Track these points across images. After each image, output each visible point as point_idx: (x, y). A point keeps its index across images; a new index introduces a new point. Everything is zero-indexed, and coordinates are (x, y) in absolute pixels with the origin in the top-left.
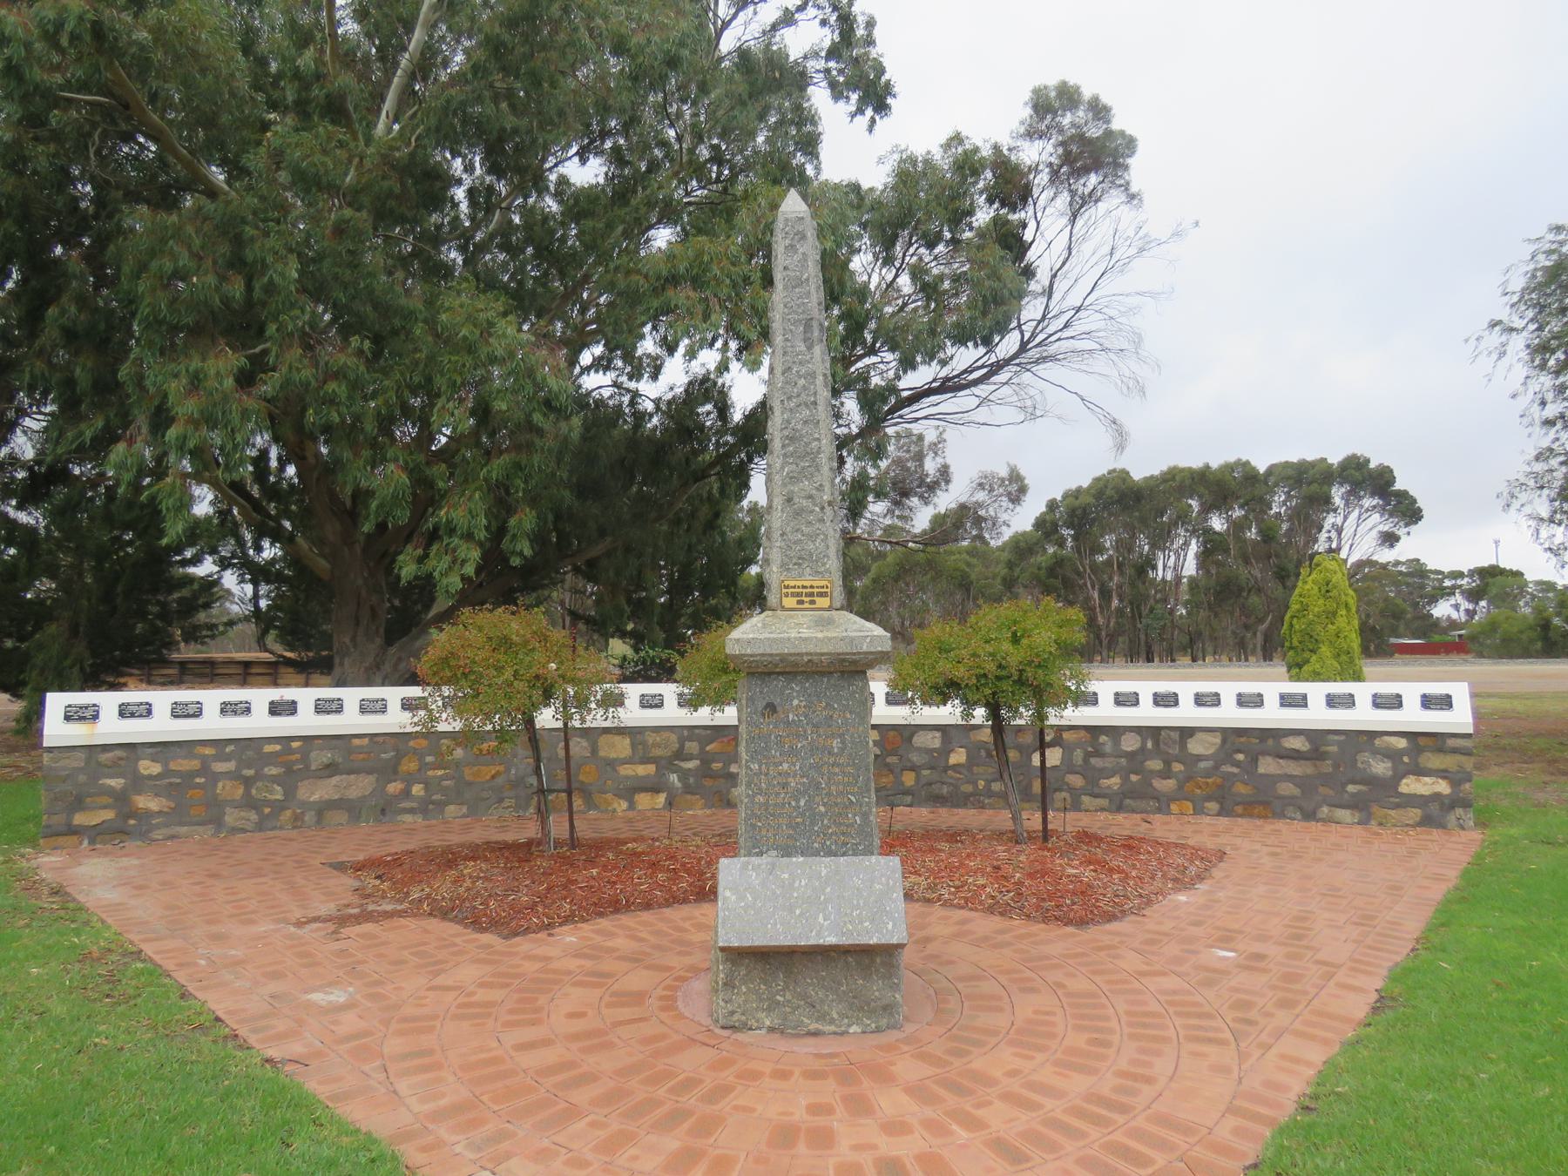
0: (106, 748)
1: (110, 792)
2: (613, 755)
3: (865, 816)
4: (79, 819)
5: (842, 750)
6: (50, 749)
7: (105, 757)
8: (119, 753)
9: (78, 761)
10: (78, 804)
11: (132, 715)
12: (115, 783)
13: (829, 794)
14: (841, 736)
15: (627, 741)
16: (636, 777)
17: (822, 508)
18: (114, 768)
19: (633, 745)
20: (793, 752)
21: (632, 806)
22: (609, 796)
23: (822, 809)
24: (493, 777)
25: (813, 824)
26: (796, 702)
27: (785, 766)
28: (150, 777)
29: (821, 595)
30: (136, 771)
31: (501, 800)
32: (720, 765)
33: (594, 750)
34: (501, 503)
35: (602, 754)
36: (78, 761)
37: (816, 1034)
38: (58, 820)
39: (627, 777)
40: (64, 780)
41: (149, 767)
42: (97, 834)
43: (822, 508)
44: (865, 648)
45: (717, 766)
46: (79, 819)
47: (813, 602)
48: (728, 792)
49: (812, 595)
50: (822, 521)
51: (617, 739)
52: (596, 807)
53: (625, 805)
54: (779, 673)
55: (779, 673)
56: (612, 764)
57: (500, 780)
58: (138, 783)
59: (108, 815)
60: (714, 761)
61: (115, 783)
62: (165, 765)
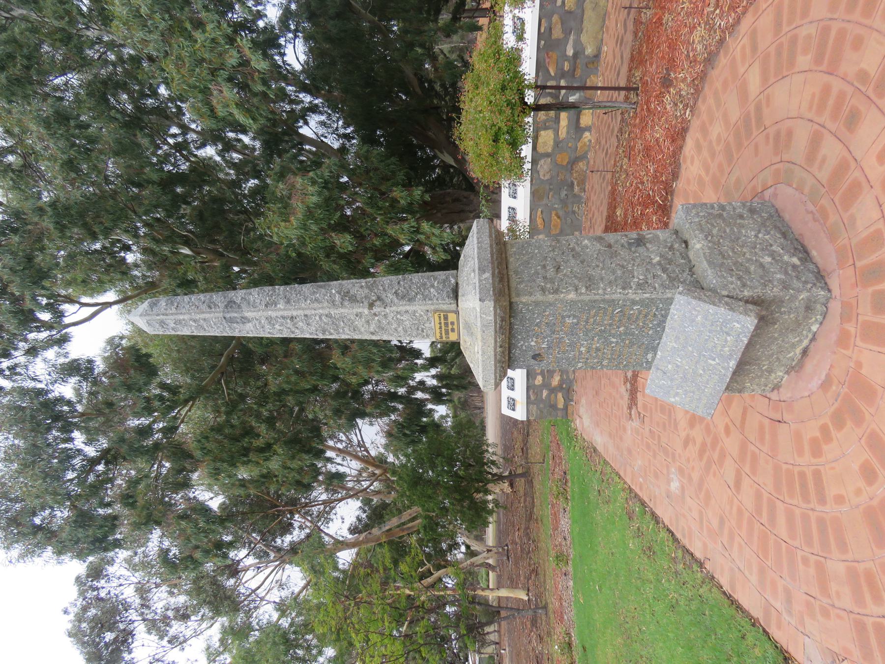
0: (528, 397)
1: (549, 396)
2: (552, 143)
3: (634, 303)
4: (561, 405)
5: (575, 317)
6: (527, 417)
7: (532, 398)
8: (531, 393)
9: (534, 408)
10: (554, 407)
11: (513, 386)
12: (545, 393)
13: (610, 325)
14: (563, 317)
15: (542, 133)
16: (568, 126)
17: (375, 315)
18: (538, 393)
19: (546, 128)
20: (572, 345)
21: (588, 129)
22: (579, 145)
23: (622, 329)
24: (559, 217)
25: (633, 334)
26: (533, 343)
27: (583, 349)
28: (543, 380)
29: (446, 318)
30: (539, 386)
31: (574, 212)
32: (566, 64)
33: (547, 155)
34: (394, 212)
35: (550, 150)
36: (534, 408)
37: (805, 352)
38: (560, 413)
39: (568, 133)
40: (542, 412)
41: (539, 380)
42: (568, 399)
43: (375, 315)
44: (492, 318)
45: (567, 67)
46: (561, 405)
47: (452, 323)
48: (588, 57)
49: (446, 324)
50: (385, 316)
51: (540, 140)
52: (586, 153)
53: (587, 134)
54: (510, 352)
55: (510, 352)
56: (557, 143)
57: (561, 213)
58: (546, 385)
59: (560, 395)
60: (563, 69)
61: (545, 393)
62: (538, 374)
